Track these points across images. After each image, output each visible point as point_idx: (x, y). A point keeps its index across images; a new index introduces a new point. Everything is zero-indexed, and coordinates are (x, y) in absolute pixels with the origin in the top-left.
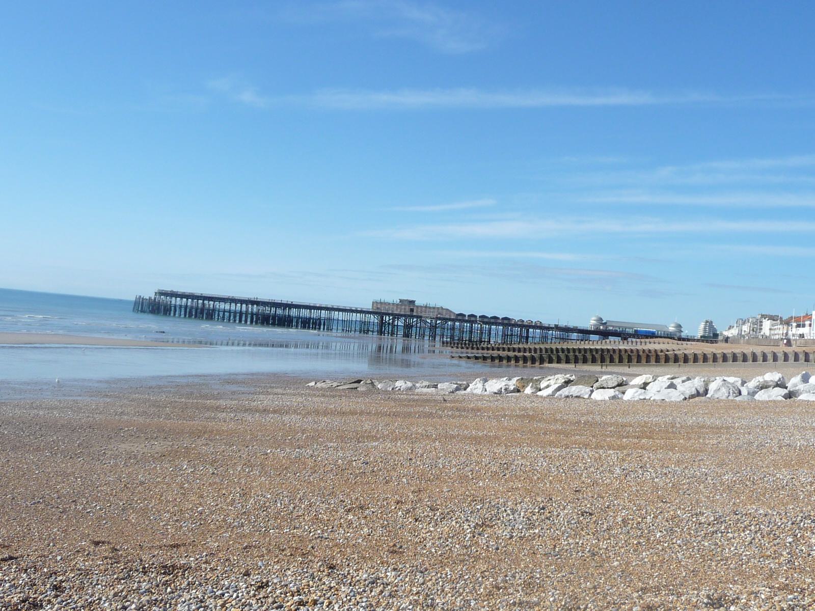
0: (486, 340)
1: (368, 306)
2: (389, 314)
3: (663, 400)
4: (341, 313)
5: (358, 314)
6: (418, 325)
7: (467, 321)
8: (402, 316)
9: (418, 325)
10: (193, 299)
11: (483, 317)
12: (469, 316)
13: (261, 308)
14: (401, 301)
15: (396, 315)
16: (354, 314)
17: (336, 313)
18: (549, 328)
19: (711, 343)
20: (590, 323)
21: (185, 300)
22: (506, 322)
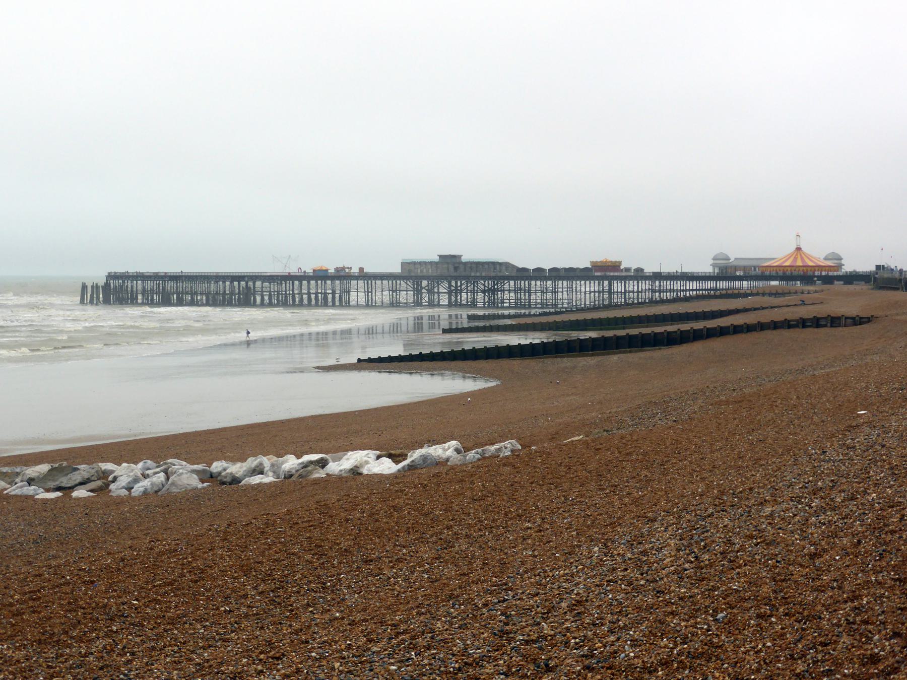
11: (554, 270)
18: (333, 278)
22: (554, 274)
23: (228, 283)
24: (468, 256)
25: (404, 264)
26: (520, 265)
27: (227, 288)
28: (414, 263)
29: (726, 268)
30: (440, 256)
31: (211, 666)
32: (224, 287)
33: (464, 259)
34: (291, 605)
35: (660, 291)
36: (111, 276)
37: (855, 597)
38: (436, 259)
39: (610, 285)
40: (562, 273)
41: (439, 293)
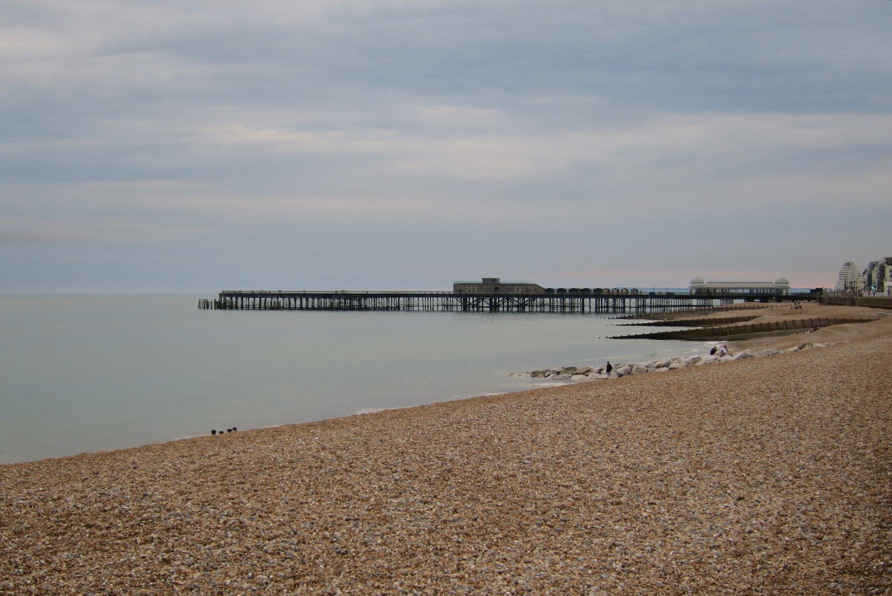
0: (648, 310)
1: (450, 289)
2: (473, 296)
3: (848, 264)
4: (420, 299)
5: (440, 299)
6: (506, 304)
7: (557, 296)
8: (487, 296)
9: (506, 304)
10: (318, 299)
11: (572, 290)
12: (595, 290)
13: (275, 299)
14: (484, 279)
15: (480, 296)
16: (435, 299)
17: (416, 299)
18: (645, 297)
19: (366, 415)
20: (683, 285)
21: (251, 299)
22: (573, 293)
23: (234, 299)
24: (506, 278)
25: (455, 285)
26: (546, 287)
27: (263, 303)
28: (465, 284)
29: (701, 289)
30: (484, 279)
31: (759, 550)
32: (313, 303)
33: (502, 281)
34: (325, 538)
35: (651, 307)
36: (224, 295)
37: (475, 520)
38: (481, 281)
39: (614, 302)
40: (579, 293)
41: (483, 307)
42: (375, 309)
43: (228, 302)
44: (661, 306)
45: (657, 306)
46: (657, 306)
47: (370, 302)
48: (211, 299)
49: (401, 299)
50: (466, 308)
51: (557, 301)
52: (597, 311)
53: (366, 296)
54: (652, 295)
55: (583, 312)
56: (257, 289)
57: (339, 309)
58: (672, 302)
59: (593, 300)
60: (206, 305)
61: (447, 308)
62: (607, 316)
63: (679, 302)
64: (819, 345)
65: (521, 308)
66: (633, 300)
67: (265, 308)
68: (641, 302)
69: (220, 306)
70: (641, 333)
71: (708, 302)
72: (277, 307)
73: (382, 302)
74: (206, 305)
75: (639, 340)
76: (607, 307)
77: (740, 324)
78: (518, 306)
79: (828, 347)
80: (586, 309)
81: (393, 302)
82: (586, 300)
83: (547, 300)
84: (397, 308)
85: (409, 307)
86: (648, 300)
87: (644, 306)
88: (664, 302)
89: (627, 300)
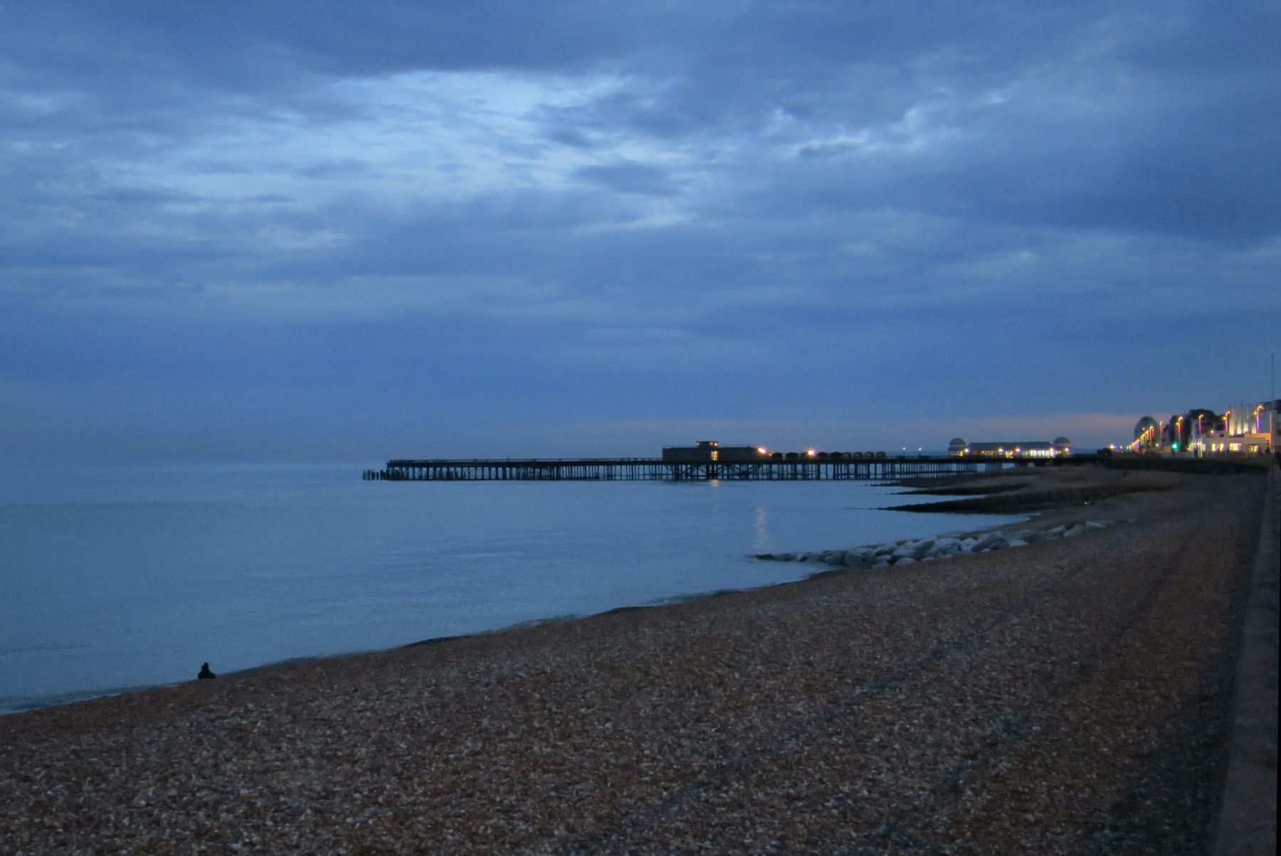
12: (788, 455)
21: (424, 469)
25: (665, 451)
36: (392, 464)
42: (570, 478)
43: (397, 471)
44: (913, 473)
45: (907, 473)
46: (907, 473)
47: (564, 471)
48: (377, 470)
49: (601, 467)
50: (677, 477)
51: (788, 468)
52: (836, 477)
53: (559, 464)
54: (902, 460)
55: (818, 478)
56: (430, 457)
57: (525, 478)
58: (926, 467)
59: (831, 467)
60: (370, 475)
61: (655, 477)
62: (868, 483)
63: (934, 467)
64: (1098, 525)
65: (744, 476)
66: (879, 466)
67: (511, 478)
68: (888, 467)
69: (385, 476)
70: (905, 504)
71: (971, 466)
72: (449, 477)
73: (579, 470)
74: (370, 475)
75: (903, 513)
76: (848, 474)
77: (1004, 494)
78: (740, 475)
79: (1033, 519)
80: (823, 476)
81: (591, 470)
82: (823, 467)
83: (775, 467)
84: (597, 478)
85: (610, 477)
86: (897, 466)
87: (893, 473)
88: (917, 467)
89: (872, 466)
